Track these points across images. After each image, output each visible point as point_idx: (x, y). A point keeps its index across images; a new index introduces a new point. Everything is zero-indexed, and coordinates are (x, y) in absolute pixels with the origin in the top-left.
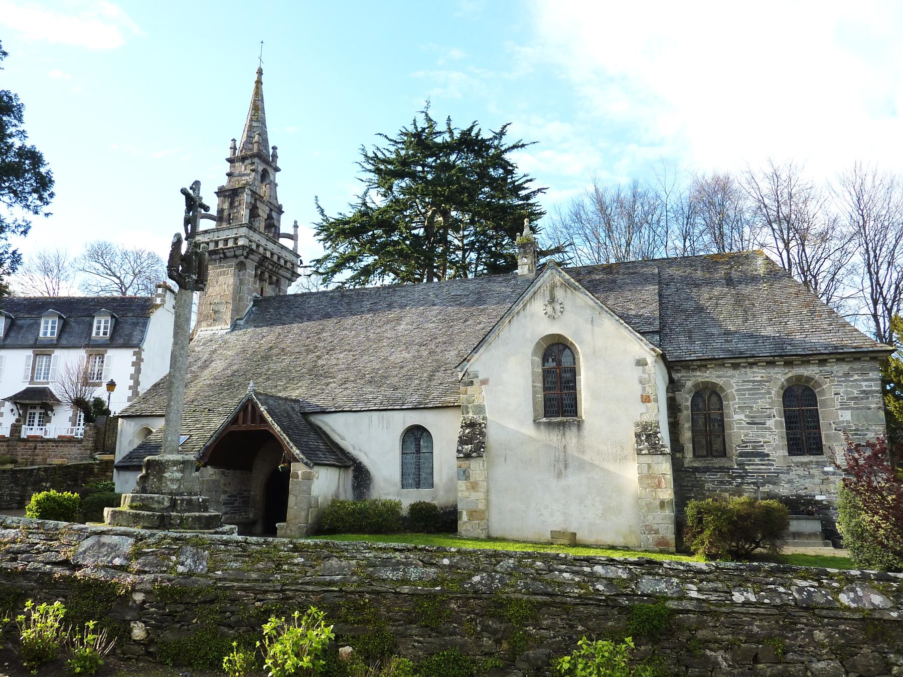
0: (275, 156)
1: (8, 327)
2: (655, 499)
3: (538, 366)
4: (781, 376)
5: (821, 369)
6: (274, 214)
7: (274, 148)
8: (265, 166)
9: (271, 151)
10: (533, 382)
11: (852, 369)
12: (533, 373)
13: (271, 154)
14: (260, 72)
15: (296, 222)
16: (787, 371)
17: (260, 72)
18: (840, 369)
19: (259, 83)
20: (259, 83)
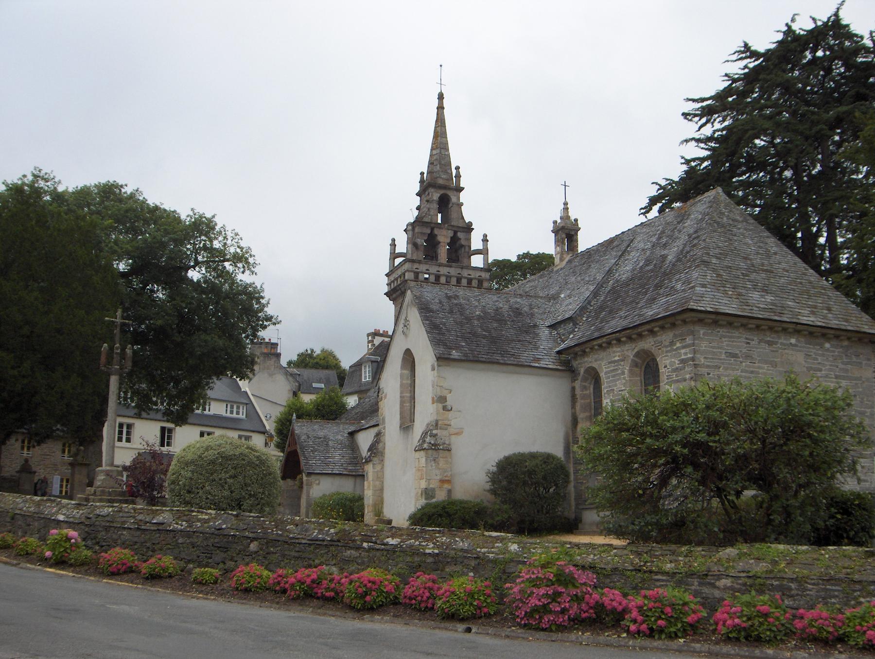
0: (458, 176)
1: (374, 370)
2: (580, 499)
3: (407, 378)
4: (630, 351)
5: (655, 339)
6: (460, 235)
7: (457, 168)
8: (442, 192)
9: (454, 172)
10: (401, 393)
11: (675, 336)
12: (402, 385)
13: (454, 175)
14: (441, 97)
15: (485, 236)
16: (634, 346)
17: (441, 97)
18: (666, 337)
19: (440, 108)
20: (440, 108)
